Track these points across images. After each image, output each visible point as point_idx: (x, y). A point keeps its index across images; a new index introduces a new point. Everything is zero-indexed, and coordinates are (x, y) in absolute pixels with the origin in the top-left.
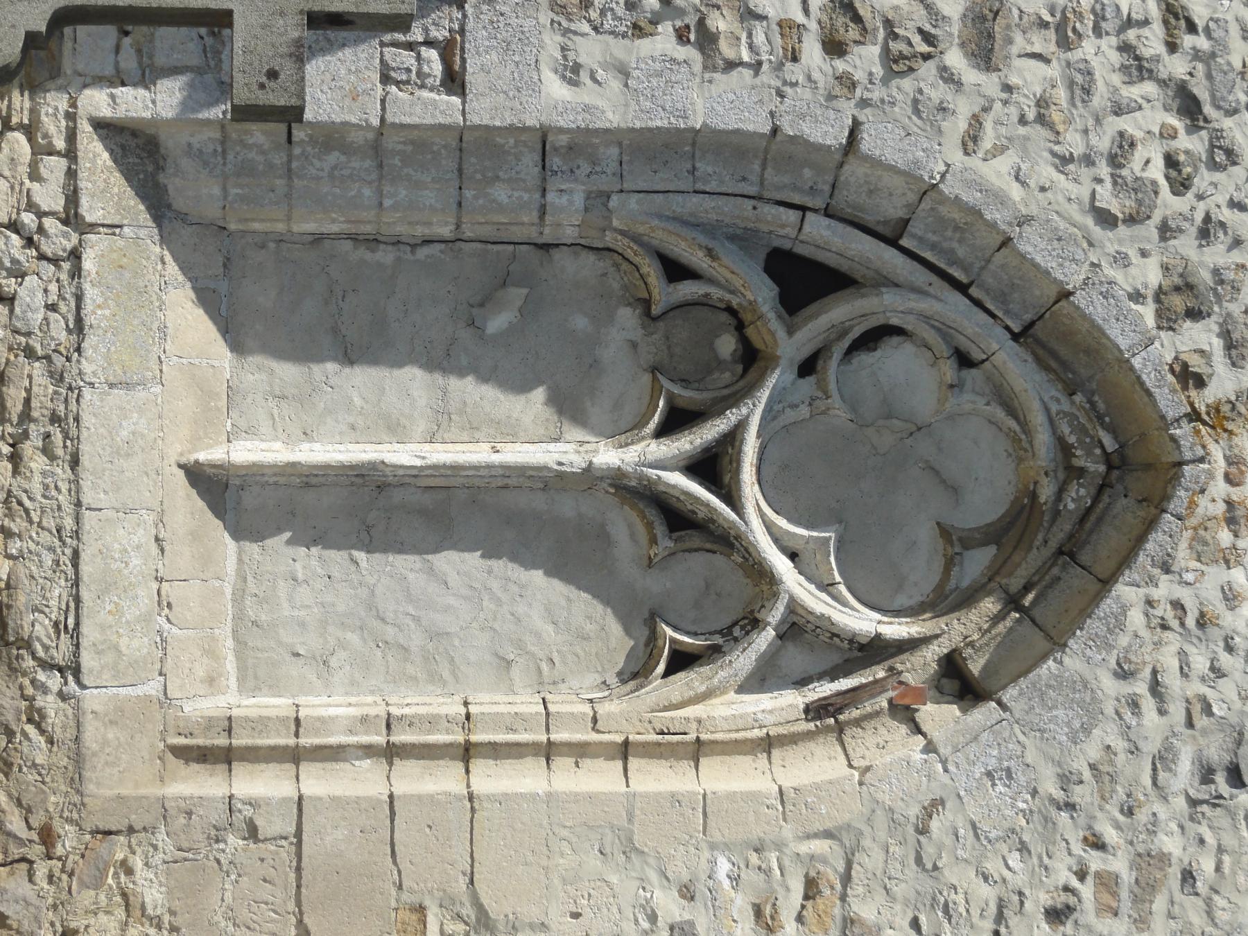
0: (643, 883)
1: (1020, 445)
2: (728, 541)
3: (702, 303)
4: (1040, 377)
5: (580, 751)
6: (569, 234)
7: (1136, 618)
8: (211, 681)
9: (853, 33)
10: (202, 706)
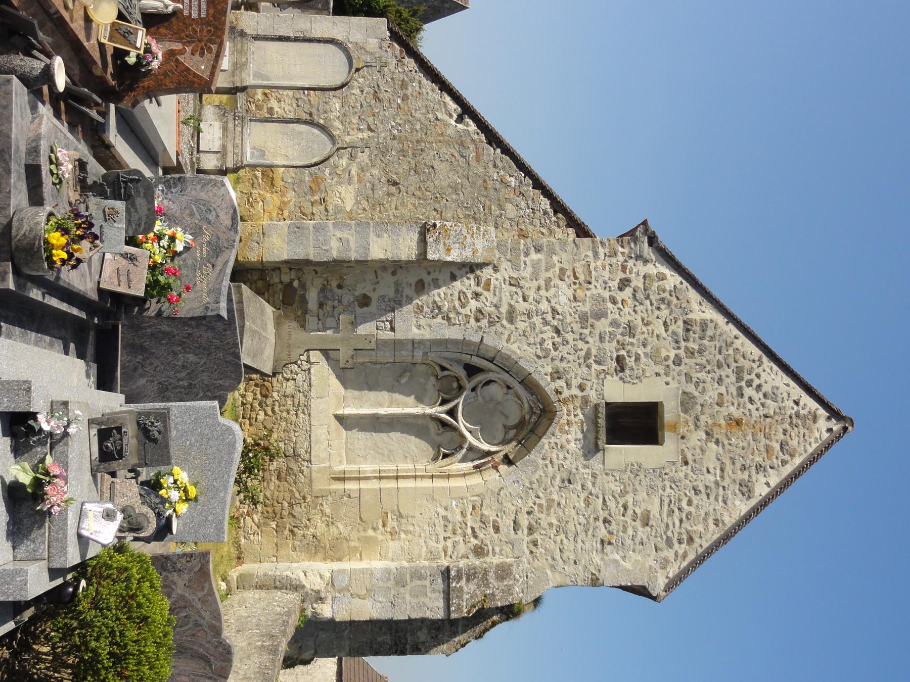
0: (436, 507)
1: (521, 407)
2: (455, 429)
3: (450, 376)
4: (525, 392)
5: (422, 477)
6: (419, 361)
7: (547, 446)
8: (340, 462)
9: (481, 317)
10: (338, 468)
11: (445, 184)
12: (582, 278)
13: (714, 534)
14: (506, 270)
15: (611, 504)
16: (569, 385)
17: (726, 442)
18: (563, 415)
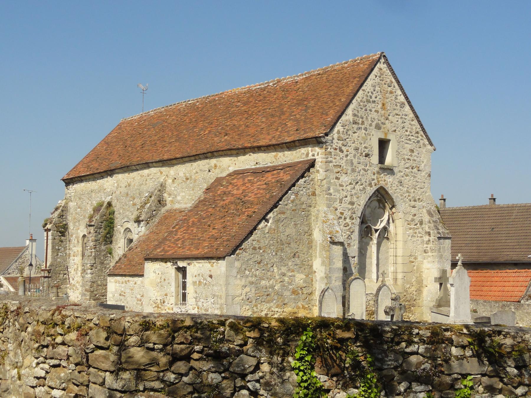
11: (294, 230)
12: (339, 169)
13: (415, 122)
14: (337, 204)
15: (407, 165)
16: (373, 180)
17: (389, 112)
18: (382, 183)
